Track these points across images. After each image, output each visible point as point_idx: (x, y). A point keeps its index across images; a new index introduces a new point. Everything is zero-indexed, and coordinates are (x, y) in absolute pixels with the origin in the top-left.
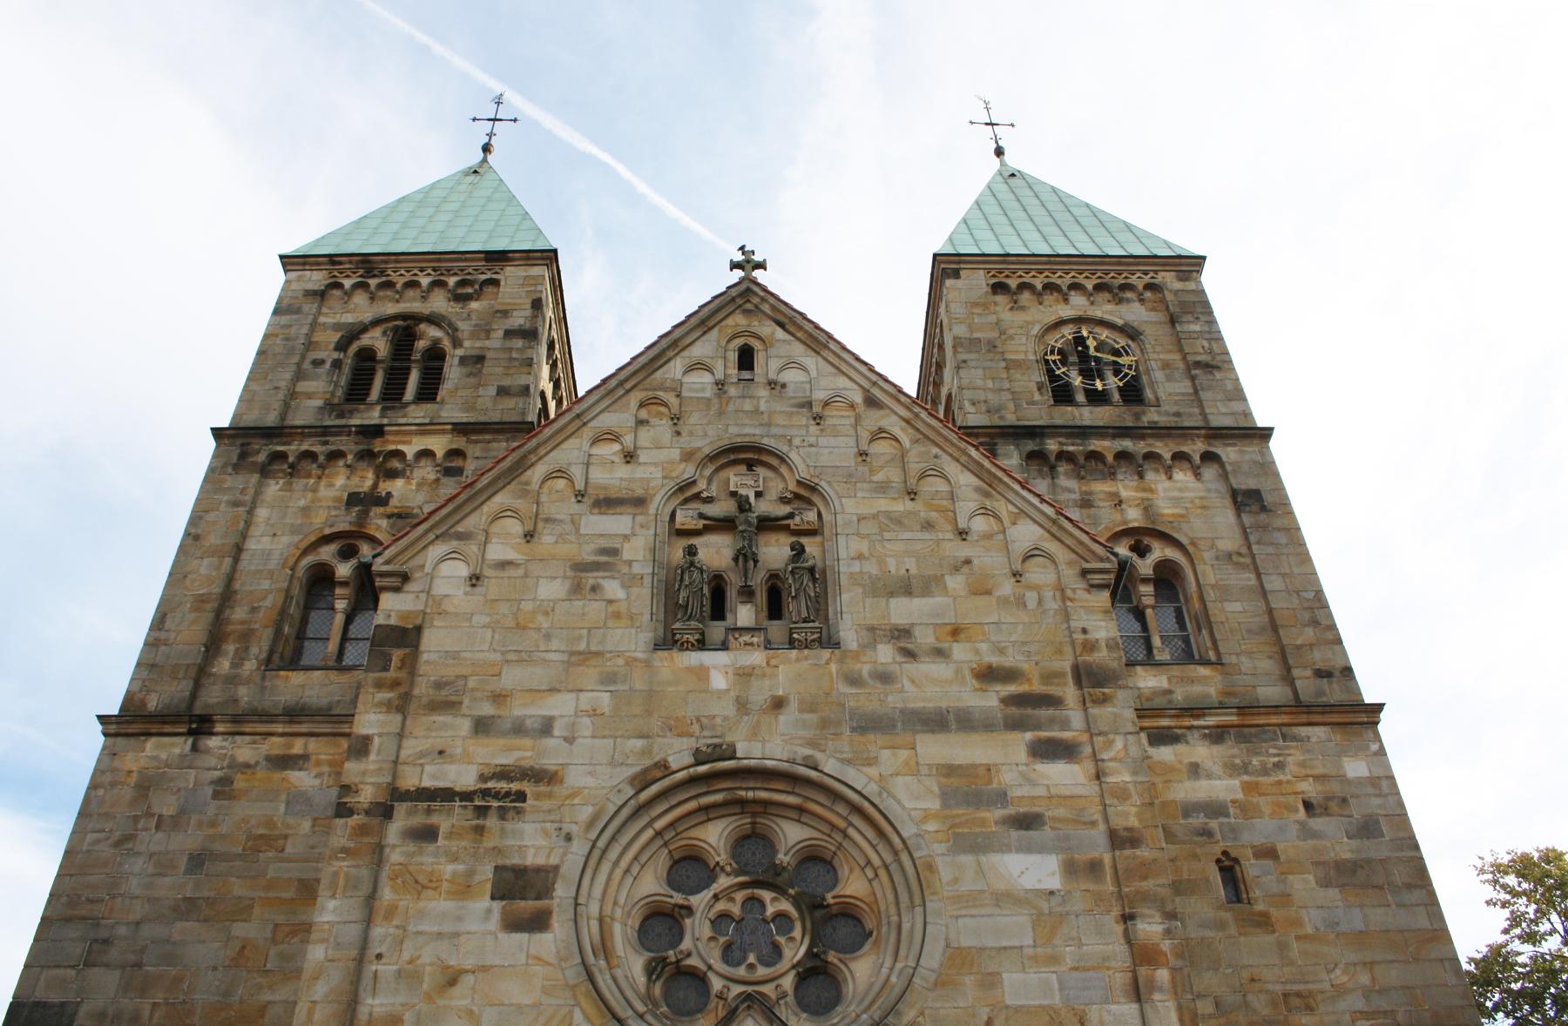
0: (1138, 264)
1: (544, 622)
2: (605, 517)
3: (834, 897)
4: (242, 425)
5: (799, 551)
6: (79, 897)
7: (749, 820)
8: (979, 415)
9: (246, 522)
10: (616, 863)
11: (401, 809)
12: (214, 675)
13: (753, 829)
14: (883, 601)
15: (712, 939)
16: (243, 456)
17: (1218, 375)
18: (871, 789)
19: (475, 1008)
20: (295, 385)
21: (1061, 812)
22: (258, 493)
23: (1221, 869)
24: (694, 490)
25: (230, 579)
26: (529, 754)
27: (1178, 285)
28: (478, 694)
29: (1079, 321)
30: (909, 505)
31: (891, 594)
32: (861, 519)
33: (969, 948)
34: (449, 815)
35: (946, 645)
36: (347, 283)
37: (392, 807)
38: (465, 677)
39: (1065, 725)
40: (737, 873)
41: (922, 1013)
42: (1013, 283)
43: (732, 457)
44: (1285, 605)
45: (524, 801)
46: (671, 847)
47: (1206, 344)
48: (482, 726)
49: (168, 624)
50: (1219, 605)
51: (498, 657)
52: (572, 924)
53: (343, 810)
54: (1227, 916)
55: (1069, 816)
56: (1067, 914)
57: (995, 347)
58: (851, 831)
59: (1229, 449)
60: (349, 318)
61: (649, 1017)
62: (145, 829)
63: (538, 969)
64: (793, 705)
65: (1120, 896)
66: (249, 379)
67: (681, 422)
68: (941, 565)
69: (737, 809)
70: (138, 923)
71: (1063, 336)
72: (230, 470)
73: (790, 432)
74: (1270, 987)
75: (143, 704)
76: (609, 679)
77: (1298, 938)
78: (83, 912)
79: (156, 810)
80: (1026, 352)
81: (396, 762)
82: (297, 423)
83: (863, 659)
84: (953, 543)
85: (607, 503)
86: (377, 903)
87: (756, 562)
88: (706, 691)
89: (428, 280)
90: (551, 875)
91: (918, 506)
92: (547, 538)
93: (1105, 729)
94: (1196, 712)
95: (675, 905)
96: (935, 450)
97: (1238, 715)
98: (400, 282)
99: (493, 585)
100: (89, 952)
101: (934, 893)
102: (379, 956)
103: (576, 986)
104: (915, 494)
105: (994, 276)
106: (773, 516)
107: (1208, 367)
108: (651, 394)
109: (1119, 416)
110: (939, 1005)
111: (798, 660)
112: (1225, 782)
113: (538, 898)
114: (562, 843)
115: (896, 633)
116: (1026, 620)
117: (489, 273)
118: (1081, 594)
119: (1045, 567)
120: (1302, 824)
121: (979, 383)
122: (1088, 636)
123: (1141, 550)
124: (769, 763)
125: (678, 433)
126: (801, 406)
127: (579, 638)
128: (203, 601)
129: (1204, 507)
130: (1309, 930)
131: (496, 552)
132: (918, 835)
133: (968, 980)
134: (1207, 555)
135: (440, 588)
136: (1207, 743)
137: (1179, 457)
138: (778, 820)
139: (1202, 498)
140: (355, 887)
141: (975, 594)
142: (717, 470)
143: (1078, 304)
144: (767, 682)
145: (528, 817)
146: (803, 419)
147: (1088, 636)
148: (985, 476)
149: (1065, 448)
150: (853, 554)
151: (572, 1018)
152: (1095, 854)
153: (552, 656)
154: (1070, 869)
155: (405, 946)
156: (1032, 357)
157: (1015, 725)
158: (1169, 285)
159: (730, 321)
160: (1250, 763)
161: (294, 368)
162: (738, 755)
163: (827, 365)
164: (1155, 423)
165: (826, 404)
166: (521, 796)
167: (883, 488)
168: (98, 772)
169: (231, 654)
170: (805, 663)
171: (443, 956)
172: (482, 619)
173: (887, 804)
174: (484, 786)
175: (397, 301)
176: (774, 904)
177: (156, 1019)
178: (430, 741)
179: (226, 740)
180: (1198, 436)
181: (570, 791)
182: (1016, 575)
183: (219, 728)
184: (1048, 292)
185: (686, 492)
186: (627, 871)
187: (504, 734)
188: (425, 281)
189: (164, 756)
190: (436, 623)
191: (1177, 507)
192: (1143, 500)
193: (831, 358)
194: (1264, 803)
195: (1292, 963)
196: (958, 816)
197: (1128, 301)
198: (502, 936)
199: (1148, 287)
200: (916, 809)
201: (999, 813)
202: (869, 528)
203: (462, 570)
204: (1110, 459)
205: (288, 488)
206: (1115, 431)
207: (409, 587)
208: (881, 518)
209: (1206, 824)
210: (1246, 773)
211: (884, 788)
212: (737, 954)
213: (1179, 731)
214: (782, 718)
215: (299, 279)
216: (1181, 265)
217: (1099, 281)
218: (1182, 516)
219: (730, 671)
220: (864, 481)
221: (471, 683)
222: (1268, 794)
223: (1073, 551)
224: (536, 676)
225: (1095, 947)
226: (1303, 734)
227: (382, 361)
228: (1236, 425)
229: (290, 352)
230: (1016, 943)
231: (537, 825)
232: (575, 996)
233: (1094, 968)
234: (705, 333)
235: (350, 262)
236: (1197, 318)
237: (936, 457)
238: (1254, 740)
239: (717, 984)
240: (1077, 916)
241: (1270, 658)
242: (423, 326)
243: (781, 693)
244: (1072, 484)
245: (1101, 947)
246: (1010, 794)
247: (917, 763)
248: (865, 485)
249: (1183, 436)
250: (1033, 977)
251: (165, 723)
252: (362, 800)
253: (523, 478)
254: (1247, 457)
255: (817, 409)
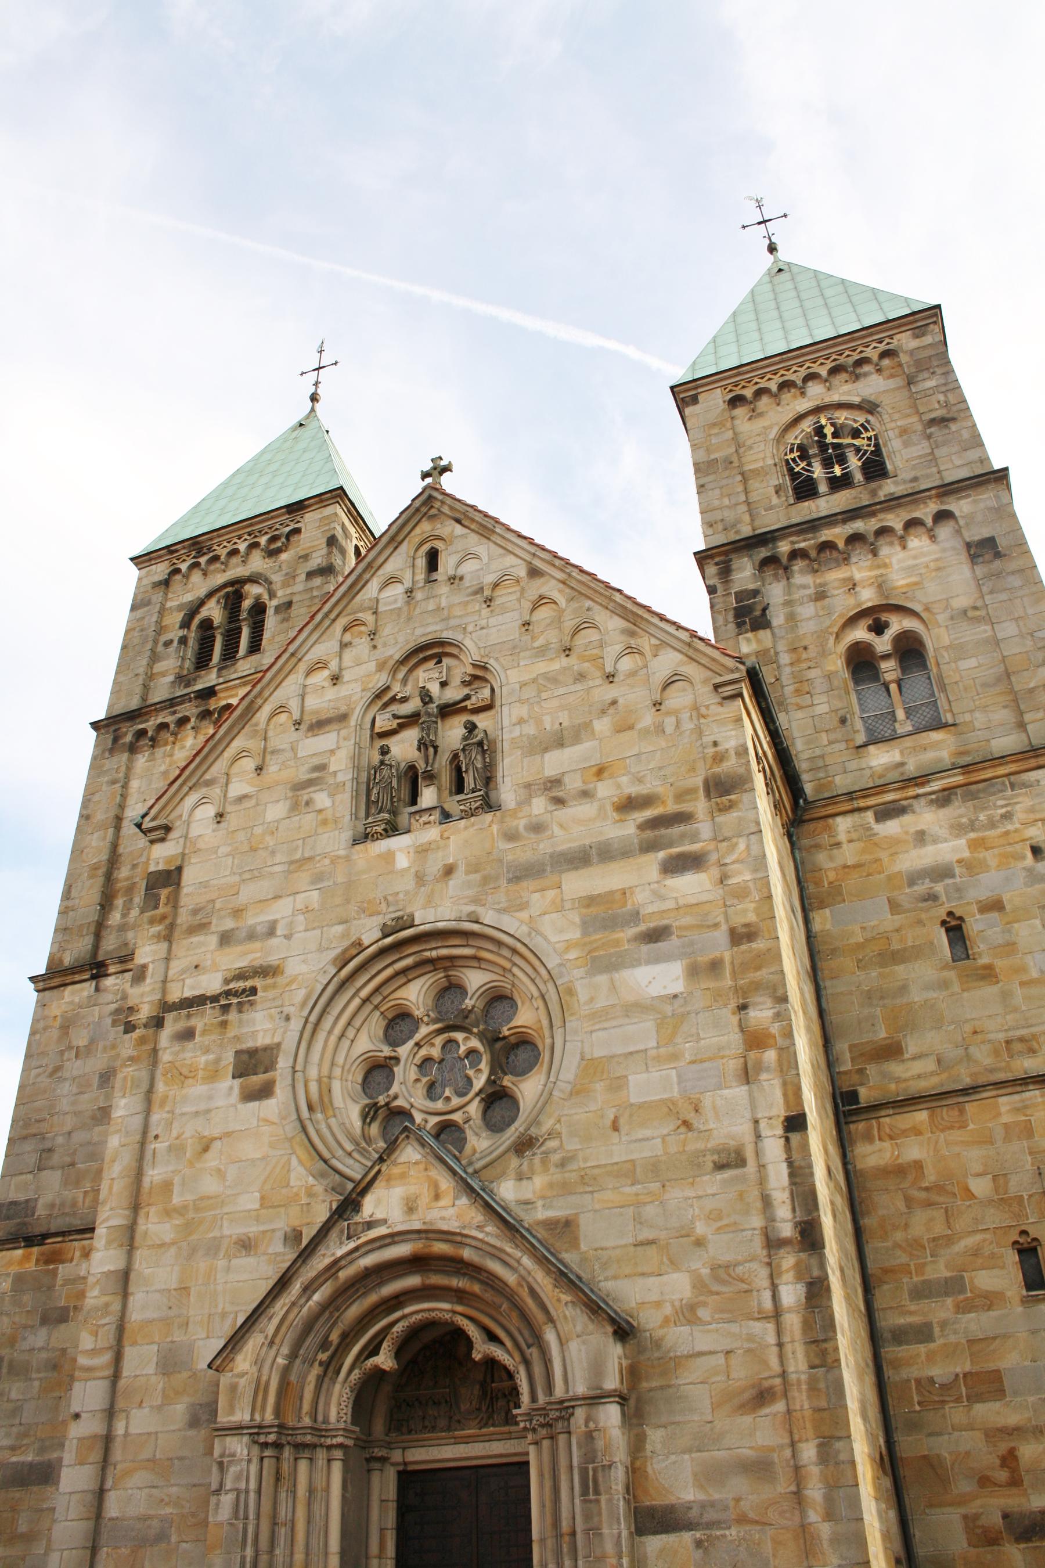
0: (871, 334)
1: (270, 841)
2: (317, 738)
3: (509, 1029)
4: (114, 714)
5: (471, 727)
6: (30, 1119)
7: (442, 975)
8: (717, 536)
9: (121, 795)
10: (330, 1032)
11: (169, 1018)
12: (110, 926)
13: (449, 981)
14: (538, 757)
15: (417, 1080)
16: (115, 740)
17: (953, 427)
18: (522, 931)
19: (222, 1167)
20: (152, 668)
21: (687, 920)
22: (129, 769)
23: (947, 930)
24: (390, 694)
25: (115, 846)
26: (258, 955)
27: (914, 344)
28: (222, 913)
29: (817, 410)
30: (564, 661)
31: (546, 750)
32: (523, 685)
33: (601, 1058)
34: (202, 1017)
35: (592, 786)
36: (184, 567)
37: (163, 1017)
38: (213, 901)
39: (694, 837)
40: (436, 1021)
41: (559, 1121)
42: (748, 393)
43: (421, 656)
44: (1018, 651)
45: (256, 994)
46: (382, 1010)
47: (941, 398)
48: (226, 939)
49: (74, 894)
50: (953, 665)
51: (237, 878)
52: (290, 1088)
53: (130, 1027)
54: (951, 975)
55: (695, 922)
56: (689, 1013)
57: (731, 463)
58: (515, 970)
59: (963, 502)
60: (189, 597)
61: (355, 1155)
62: (69, 1060)
63: (266, 1129)
64: (461, 869)
65: (736, 989)
66: (116, 673)
67: (377, 637)
68: (590, 713)
69: (431, 968)
70: (69, 1133)
71: (803, 431)
72: (107, 754)
73: (465, 620)
74: (992, 1036)
75: (61, 961)
76: (318, 878)
77: (1022, 984)
78: (33, 1131)
79: (75, 1043)
80: (764, 459)
81: (165, 982)
82: (157, 700)
83: (520, 815)
84: (602, 688)
85: (319, 725)
86: (154, 1096)
87: (436, 748)
88: (392, 872)
89: (246, 544)
90: (275, 1052)
91: (573, 660)
92: (272, 768)
93: (727, 834)
94: (919, 781)
95: (386, 1058)
96: (588, 603)
97: (963, 774)
98: (223, 553)
99: (233, 821)
100: (40, 1160)
101: (572, 1014)
102: (156, 1137)
103: (293, 1137)
104: (570, 650)
105: (731, 391)
106: (451, 702)
107: (943, 421)
108: (352, 618)
109: (855, 498)
110: (573, 1111)
111: (466, 828)
112: (951, 844)
113: (265, 1072)
114: (283, 1024)
115: (549, 785)
116: (664, 744)
117: (292, 524)
118: (715, 709)
119: (684, 690)
120: (1030, 871)
121: (716, 503)
122: (718, 749)
123: (879, 628)
124: (441, 925)
125: (375, 647)
126: (476, 593)
127: (296, 849)
128: (96, 869)
129: (938, 569)
130: (1034, 974)
131: (236, 789)
132: (561, 965)
133: (599, 1086)
134: (941, 618)
135: (195, 831)
136: (933, 809)
137: (912, 524)
138: (464, 970)
139: (937, 560)
140: (138, 1086)
141: (619, 731)
142: (411, 670)
143: (816, 393)
144: (440, 854)
145: (259, 1007)
146: (477, 605)
147: (718, 749)
148: (630, 617)
149: (797, 546)
150: (514, 720)
151: (290, 1164)
152: (716, 954)
153: (277, 869)
154: (693, 972)
155: (174, 1126)
156: (770, 462)
157: (649, 847)
158: (904, 347)
159: (418, 530)
160: (977, 819)
161: (148, 653)
162: (416, 923)
163: (497, 548)
164: (891, 494)
165: (496, 585)
166: (253, 991)
167: (541, 652)
168: (35, 1021)
169: (120, 907)
170: (471, 830)
171: (200, 1129)
172: (223, 850)
173: (536, 942)
174: (227, 988)
175: (224, 571)
176: (466, 1042)
177: (87, 1204)
178: (189, 959)
179: (117, 978)
180: (930, 498)
181: (288, 980)
182: (657, 704)
183: (112, 969)
184: (786, 390)
185: (383, 697)
186: (342, 1035)
187: (241, 942)
188: (242, 547)
189: (77, 1000)
190: (193, 861)
191: (911, 576)
192: (877, 577)
193: (499, 541)
194: (990, 857)
195: (1015, 1010)
196: (596, 940)
197: (866, 375)
198: (240, 1106)
199: (885, 354)
200: (559, 942)
201: (632, 931)
202: (529, 692)
203: (209, 811)
204: (841, 545)
205: (152, 759)
206: (844, 516)
207: (172, 835)
208: (540, 681)
209: (931, 888)
210: (973, 830)
211: (534, 930)
212: (439, 1090)
213: (904, 803)
214: (451, 883)
215: (148, 575)
216: (916, 321)
217: (833, 364)
218: (916, 584)
219: (411, 850)
220: (527, 649)
221: (218, 905)
222: (993, 848)
223: (708, 668)
224: (262, 888)
225: (711, 1039)
226: (1032, 779)
227: (218, 627)
228: (972, 475)
229: (144, 642)
230: (642, 1047)
231: (265, 1012)
232: (292, 1147)
233: (710, 1059)
234: (396, 548)
235: (184, 548)
236: (933, 373)
237: (588, 609)
238: (981, 795)
239: (418, 1117)
240: (697, 1014)
241: (1005, 707)
242: (247, 587)
243: (451, 861)
244: (808, 579)
245: (716, 1039)
246: (642, 912)
247: (562, 900)
248: (528, 653)
249: (915, 502)
250: (655, 1075)
251: (74, 974)
252: (141, 1016)
253: (254, 720)
254: (982, 505)
255: (487, 593)
